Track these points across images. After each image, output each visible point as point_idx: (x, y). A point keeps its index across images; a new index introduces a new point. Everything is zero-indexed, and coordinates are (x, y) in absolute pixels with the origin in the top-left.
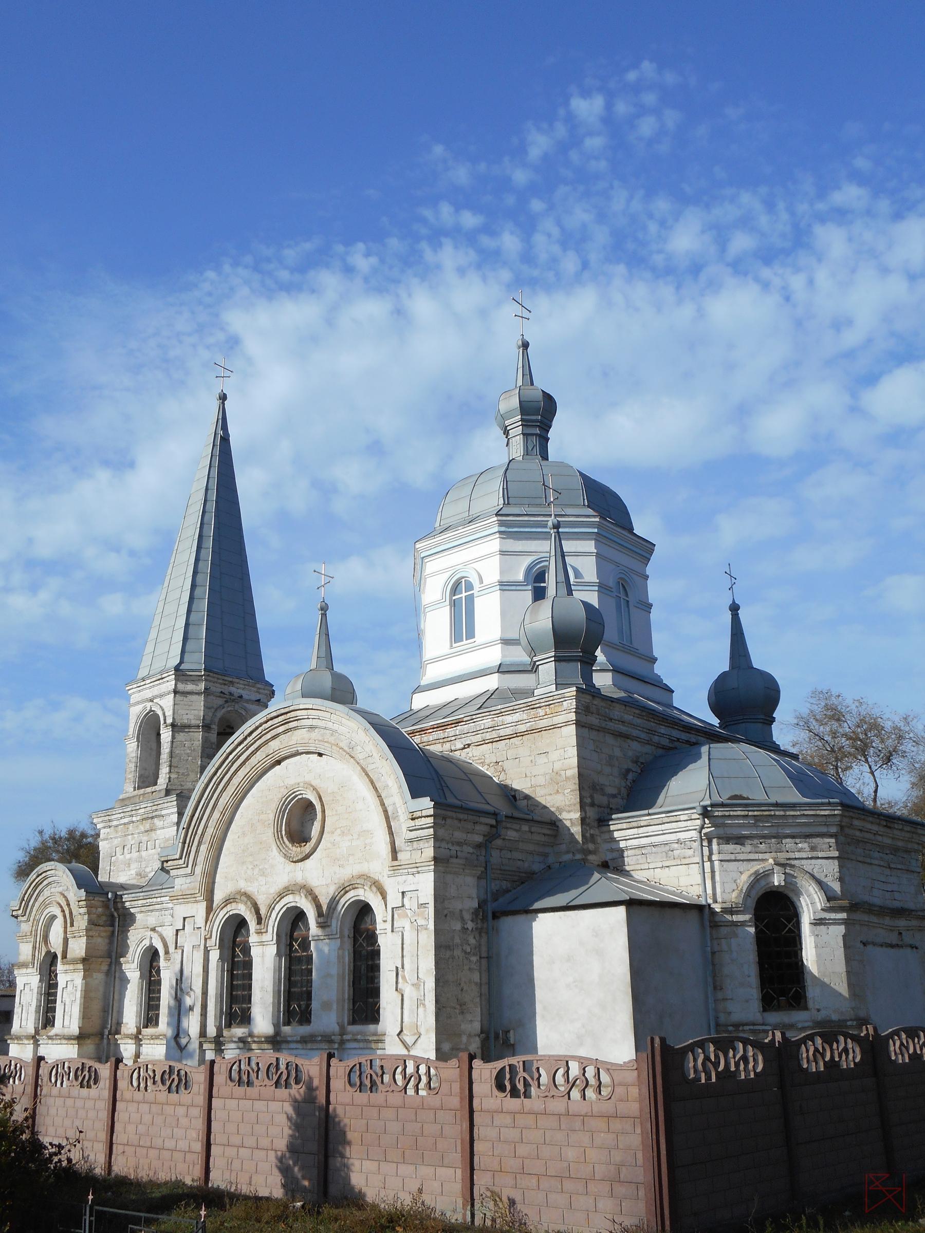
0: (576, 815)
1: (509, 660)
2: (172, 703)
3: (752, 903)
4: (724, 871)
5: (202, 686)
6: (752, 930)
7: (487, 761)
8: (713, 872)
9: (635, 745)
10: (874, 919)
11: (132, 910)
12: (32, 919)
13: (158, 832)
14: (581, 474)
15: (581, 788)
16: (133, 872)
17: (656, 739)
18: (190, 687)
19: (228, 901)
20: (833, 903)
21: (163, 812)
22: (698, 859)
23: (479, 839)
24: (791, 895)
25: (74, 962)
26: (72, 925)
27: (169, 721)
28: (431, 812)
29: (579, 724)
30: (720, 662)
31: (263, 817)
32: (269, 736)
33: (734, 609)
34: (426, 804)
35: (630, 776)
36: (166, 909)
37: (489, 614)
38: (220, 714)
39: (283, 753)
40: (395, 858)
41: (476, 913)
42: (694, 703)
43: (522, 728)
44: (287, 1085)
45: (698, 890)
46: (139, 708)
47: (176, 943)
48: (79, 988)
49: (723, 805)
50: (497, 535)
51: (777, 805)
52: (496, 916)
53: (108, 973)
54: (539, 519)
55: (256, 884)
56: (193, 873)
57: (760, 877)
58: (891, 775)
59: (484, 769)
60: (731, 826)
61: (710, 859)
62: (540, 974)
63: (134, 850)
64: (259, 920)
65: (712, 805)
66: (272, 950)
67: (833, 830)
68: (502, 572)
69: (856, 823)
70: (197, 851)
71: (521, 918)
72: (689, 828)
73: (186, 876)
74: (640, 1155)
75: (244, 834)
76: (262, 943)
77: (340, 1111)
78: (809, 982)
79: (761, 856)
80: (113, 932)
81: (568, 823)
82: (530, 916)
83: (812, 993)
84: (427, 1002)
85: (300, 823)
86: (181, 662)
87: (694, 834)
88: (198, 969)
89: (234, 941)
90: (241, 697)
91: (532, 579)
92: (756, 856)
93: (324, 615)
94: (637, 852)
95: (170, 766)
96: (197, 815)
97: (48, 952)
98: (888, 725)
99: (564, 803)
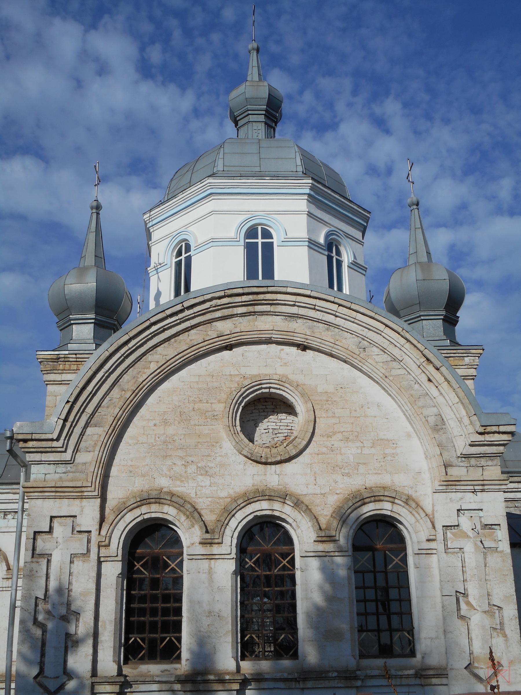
31: (204, 406)
32: (218, 314)
47: (34, 549)
50: (306, 197)
54: (336, 196)
68: (309, 231)
84: (508, 631)
96: (90, 388)
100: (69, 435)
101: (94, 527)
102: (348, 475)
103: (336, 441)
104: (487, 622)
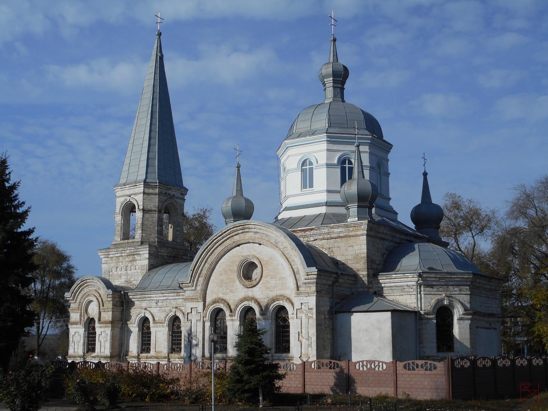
0: (365, 273)
1: (330, 200)
2: (142, 199)
3: (435, 311)
4: (425, 298)
5: (157, 191)
6: (435, 321)
7: (325, 247)
8: (421, 298)
9: (387, 243)
10: (481, 318)
11: (133, 300)
12: (78, 302)
13: (137, 262)
14: (363, 112)
15: (368, 262)
16: (123, 280)
17: (395, 239)
18: (151, 191)
19: (214, 302)
20: (467, 312)
21: (140, 253)
22: (415, 293)
23: (330, 283)
24: (451, 308)
25: (106, 323)
26: (103, 306)
27: (141, 207)
28: (316, 273)
29: (368, 235)
30: (418, 201)
31: (231, 268)
32: (234, 234)
33: (425, 174)
34: (314, 270)
35: (385, 256)
36: (153, 300)
37: (321, 177)
38: (165, 205)
39: (241, 242)
40: (298, 290)
41: (329, 312)
42: (405, 219)
43: (342, 235)
44: (334, 368)
45: (416, 306)
46: (122, 199)
48: (109, 335)
49: (427, 272)
51: (448, 273)
52: (337, 313)
53: (122, 328)
55: (228, 296)
56: (196, 289)
57: (440, 301)
58: (483, 239)
59: (324, 250)
60: (429, 280)
61: (420, 293)
62: (353, 336)
63: (123, 270)
64: (231, 311)
65: (423, 273)
66: (237, 323)
67: (469, 283)
68: (327, 159)
69: (478, 280)
70: (198, 280)
71: (347, 314)
72: (412, 280)
73: (192, 290)
74: (444, 383)
75: (221, 274)
76: (232, 320)
77: (353, 375)
78: (455, 342)
79: (440, 293)
80: (123, 309)
81: (361, 276)
82: (350, 314)
83: (456, 346)
85: (248, 270)
86: (146, 178)
87: (414, 283)
88: (200, 329)
89: (216, 319)
90: (174, 196)
91: (340, 163)
92: (438, 293)
93: (239, 170)
94: (389, 288)
95: (142, 230)
96: (198, 265)
97: (89, 318)
98: (483, 214)
99: (360, 268)
100: (193, 281)
101: (202, 311)
102: (272, 291)
103: (268, 279)
104: (307, 342)
